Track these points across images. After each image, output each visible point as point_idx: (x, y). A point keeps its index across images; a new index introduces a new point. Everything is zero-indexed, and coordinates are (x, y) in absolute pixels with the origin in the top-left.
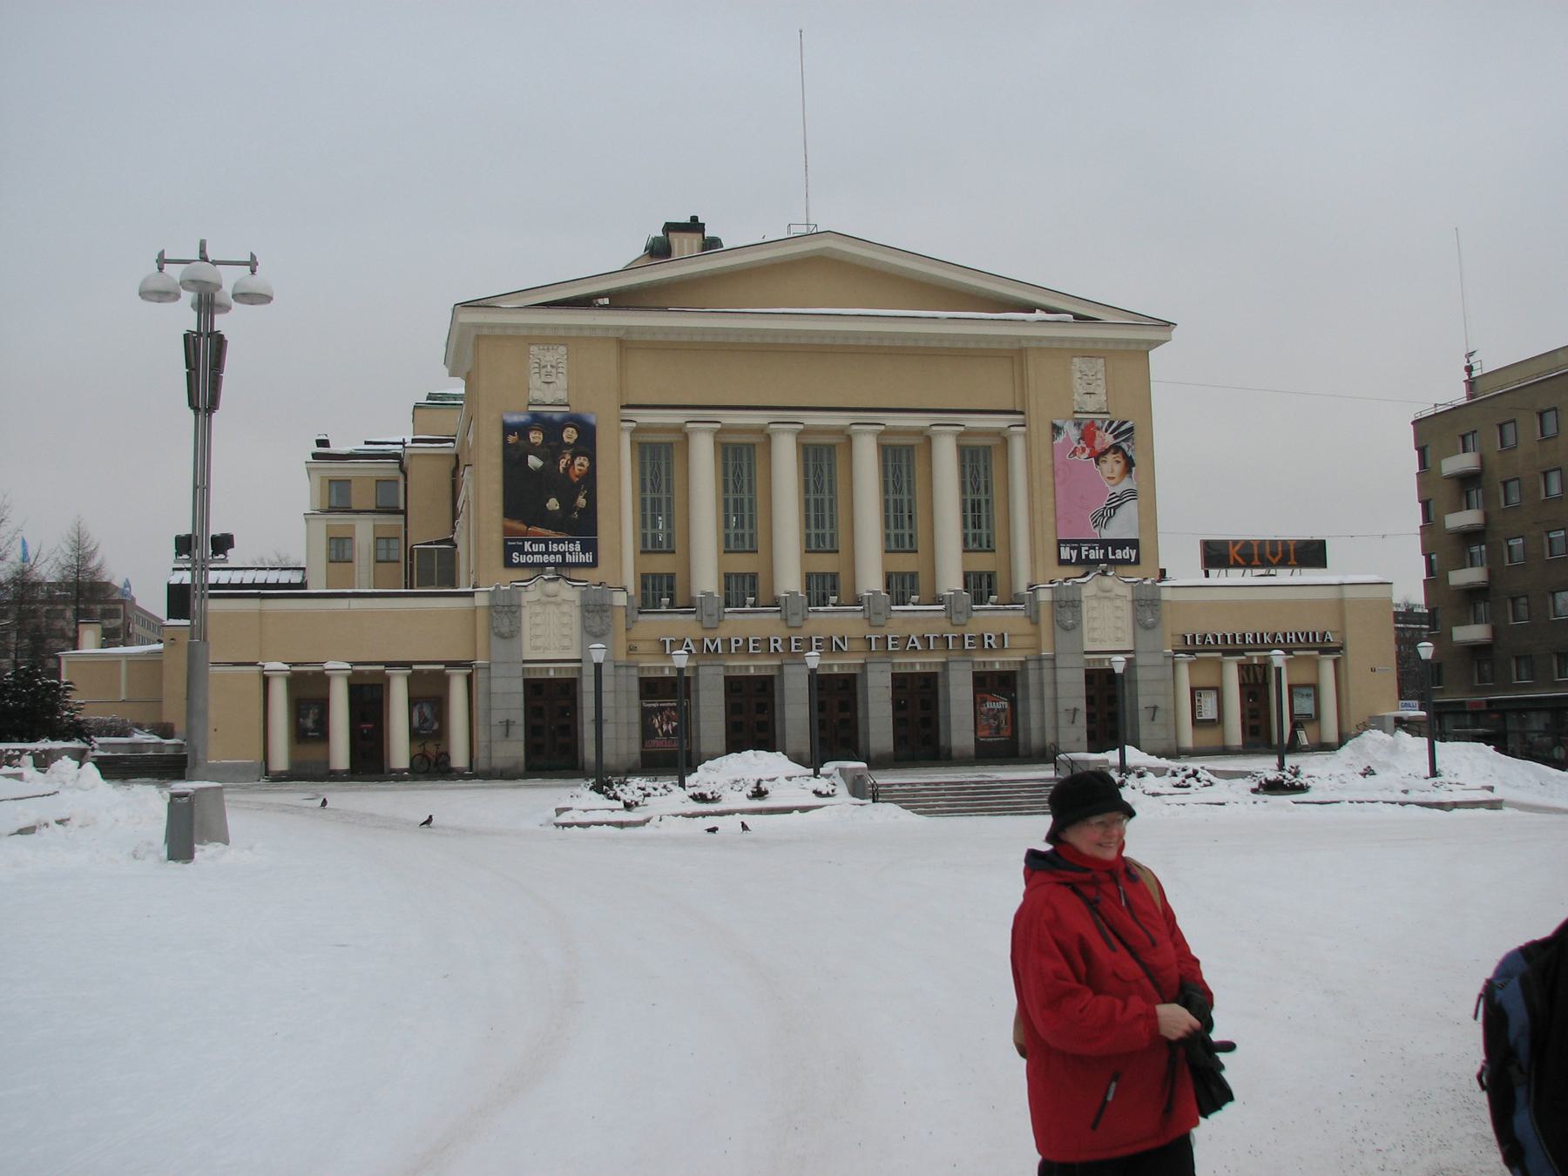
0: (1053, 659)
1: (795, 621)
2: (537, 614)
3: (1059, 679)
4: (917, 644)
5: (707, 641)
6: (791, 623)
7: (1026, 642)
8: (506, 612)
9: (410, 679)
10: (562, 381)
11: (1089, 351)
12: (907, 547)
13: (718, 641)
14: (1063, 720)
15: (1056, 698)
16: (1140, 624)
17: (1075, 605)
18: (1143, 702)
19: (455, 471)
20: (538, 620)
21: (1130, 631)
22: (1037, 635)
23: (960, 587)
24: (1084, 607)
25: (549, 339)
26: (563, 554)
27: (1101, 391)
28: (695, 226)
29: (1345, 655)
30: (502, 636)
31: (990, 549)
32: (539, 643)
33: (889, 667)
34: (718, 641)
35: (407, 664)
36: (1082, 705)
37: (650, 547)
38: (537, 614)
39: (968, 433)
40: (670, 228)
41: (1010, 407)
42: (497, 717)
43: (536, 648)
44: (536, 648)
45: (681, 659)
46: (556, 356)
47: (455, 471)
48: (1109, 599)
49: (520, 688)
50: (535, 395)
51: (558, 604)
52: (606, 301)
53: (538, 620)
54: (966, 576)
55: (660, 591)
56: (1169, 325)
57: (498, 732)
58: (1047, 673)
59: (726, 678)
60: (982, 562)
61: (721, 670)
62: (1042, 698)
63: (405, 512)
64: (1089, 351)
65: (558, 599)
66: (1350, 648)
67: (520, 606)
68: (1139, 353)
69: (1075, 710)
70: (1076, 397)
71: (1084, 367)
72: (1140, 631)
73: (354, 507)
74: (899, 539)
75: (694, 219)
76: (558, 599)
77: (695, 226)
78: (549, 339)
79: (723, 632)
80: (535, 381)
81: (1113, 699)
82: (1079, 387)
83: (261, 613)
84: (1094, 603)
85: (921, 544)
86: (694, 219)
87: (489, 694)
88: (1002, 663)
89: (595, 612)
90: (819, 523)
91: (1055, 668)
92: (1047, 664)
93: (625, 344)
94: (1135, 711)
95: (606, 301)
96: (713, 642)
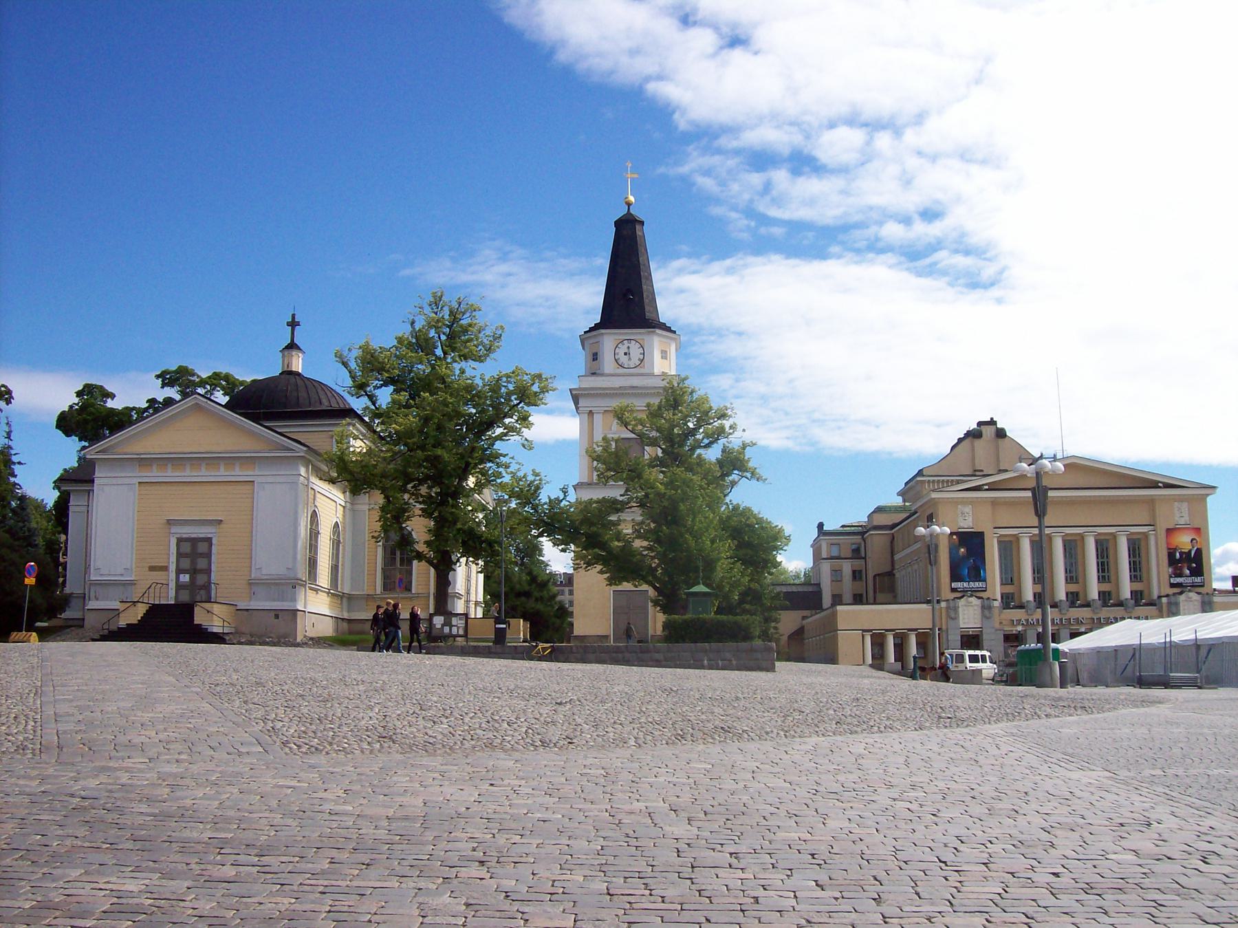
8: (952, 613)
11: (1181, 499)
16: (984, 617)
17: (956, 609)
25: (964, 502)
26: (477, 603)
28: (992, 422)
31: (1141, 581)
39: (1100, 534)
40: (980, 424)
45: (1020, 628)
46: (968, 509)
50: (962, 525)
54: (1035, 595)
55: (1010, 601)
64: (1181, 499)
68: (1202, 499)
74: (1071, 578)
78: (964, 502)
80: (960, 519)
82: (1177, 514)
85: (1113, 578)
89: (986, 608)
90: (1103, 571)
93: (994, 503)
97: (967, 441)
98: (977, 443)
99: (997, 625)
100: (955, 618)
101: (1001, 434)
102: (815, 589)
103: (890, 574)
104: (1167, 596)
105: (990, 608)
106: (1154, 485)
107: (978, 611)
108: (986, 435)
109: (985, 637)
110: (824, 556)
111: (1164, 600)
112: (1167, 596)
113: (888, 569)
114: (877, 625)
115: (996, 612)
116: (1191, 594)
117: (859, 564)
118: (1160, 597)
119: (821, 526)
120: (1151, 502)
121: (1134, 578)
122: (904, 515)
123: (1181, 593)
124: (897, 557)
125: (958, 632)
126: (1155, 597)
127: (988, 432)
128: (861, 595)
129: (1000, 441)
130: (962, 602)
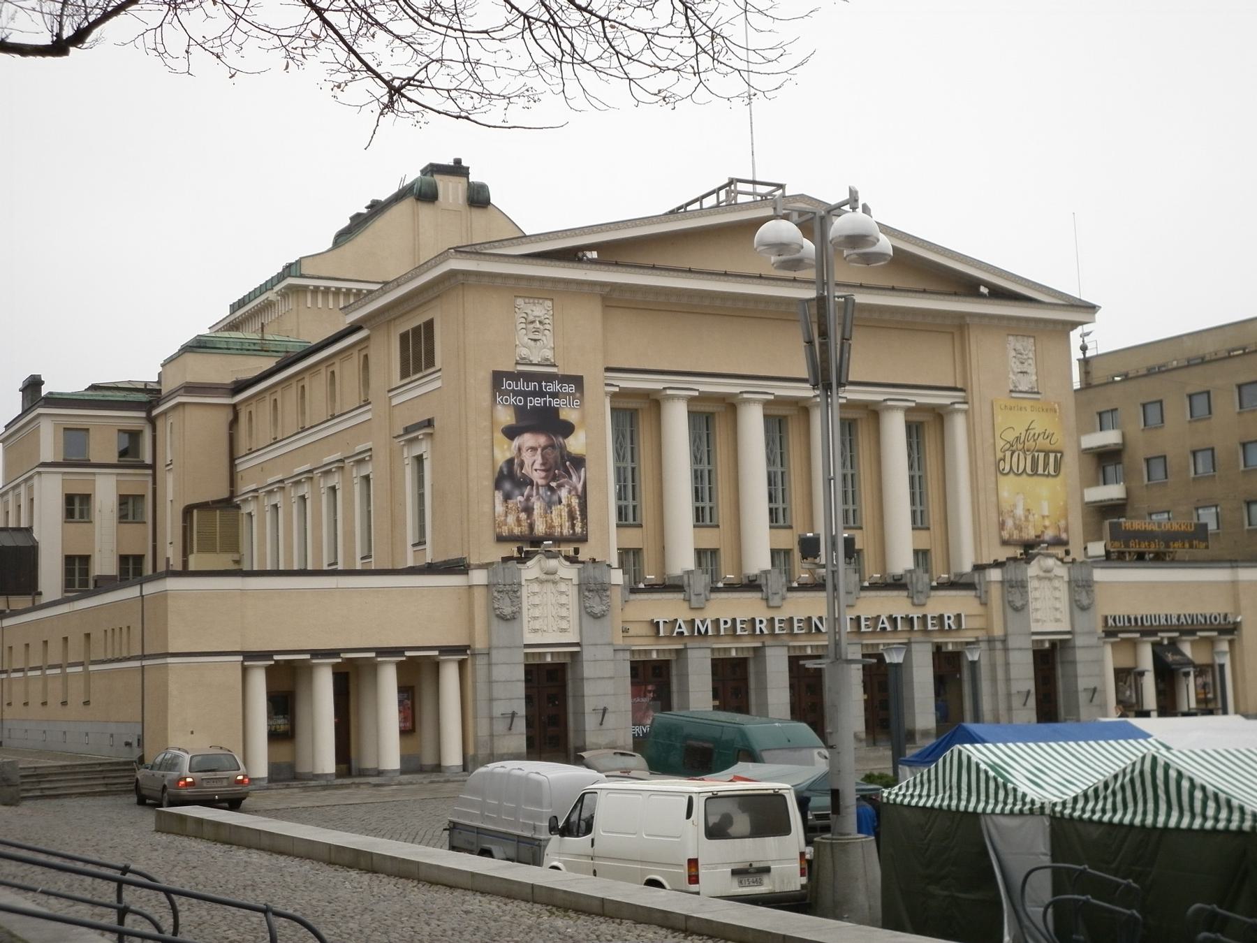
0: (1004, 641)
1: (775, 601)
2: (534, 594)
3: (1011, 660)
4: (684, 629)
5: (698, 622)
6: (916, 601)
7: (978, 623)
8: (504, 604)
9: (269, 670)
10: (547, 339)
12: (631, 521)
13: (708, 622)
14: (1017, 702)
15: (1008, 680)
18: (590, 704)
19: (234, 422)
20: (537, 600)
21: (576, 621)
22: (988, 617)
23: (768, 566)
24: (524, 592)
27: (1032, 370)
28: (458, 170)
29: (1240, 636)
30: (502, 618)
32: (537, 625)
33: (859, 647)
34: (708, 622)
35: (398, 651)
36: (520, 708)
37: (852, 524)
38: (534, 594)
40: (434, 169)
41: (951, 384)
42: (500, 708)
43: (536, 631)
44: (536, 631)
47: (234, 422)
48: (1050, 579)
49: (521, 674)
51: (555, 583)
52: (594, 255)
53: (537, 600)
56: (1092, 308)
57: (500, 727)
58: (999, 656)
59: (713, 660)
60: (710, 539)
61: (708, 654)
62: (994, 680)
63: (153, 467)
65: (557, 577)
66: (1246, 631)
67: (520, 585)
69: (513, 715)
70: (1011, 376)
71: (1019, 347)
72: (1077, 612)
73: (93, 461)
75: (458, 162)
76: (1052, 575)
77: (458, 170)
79: (710, 614)
80: (523, 337)
81: (884, 687)
83: (1234, 583)
84: (535, 587)
86: (458, 162)
87: (490, 682)
88: (955, 644)
89: (591, 588)
91: (490, 664)
92: (999, 645)
93: (612, 298)
94: (581, 714)
95: (594, 255)
96: (703, 622)
97: (407, 205)
98: (425, 210)
99: (619, 641)
100: (511, 619)
101: (478, 198)
102: (20, 541)
103: (229, 504)
104: (997, 564)
105: (602, 589)
106: (967, 286)
107: (1063, 593)
108: (43, 383)
109: (588, 670)
110: (47, 455)
111: (995, 575)
112: (997, 564)
113: (226, 495)
114: (289, 637)
115: (616, 596)
116: (553, 563)
117: (136, 482)
118: (979, 568)
119: (33, 385)
120: (959, 326)
121: (919, 522)
122: (268, 363)
123: (523, 558)
124: (243, 465)
125: (520, 658)
126: (967, 567)
127: (451, 189)
128: (139, 559)
129: (477, 214)
130: (531, 570)
